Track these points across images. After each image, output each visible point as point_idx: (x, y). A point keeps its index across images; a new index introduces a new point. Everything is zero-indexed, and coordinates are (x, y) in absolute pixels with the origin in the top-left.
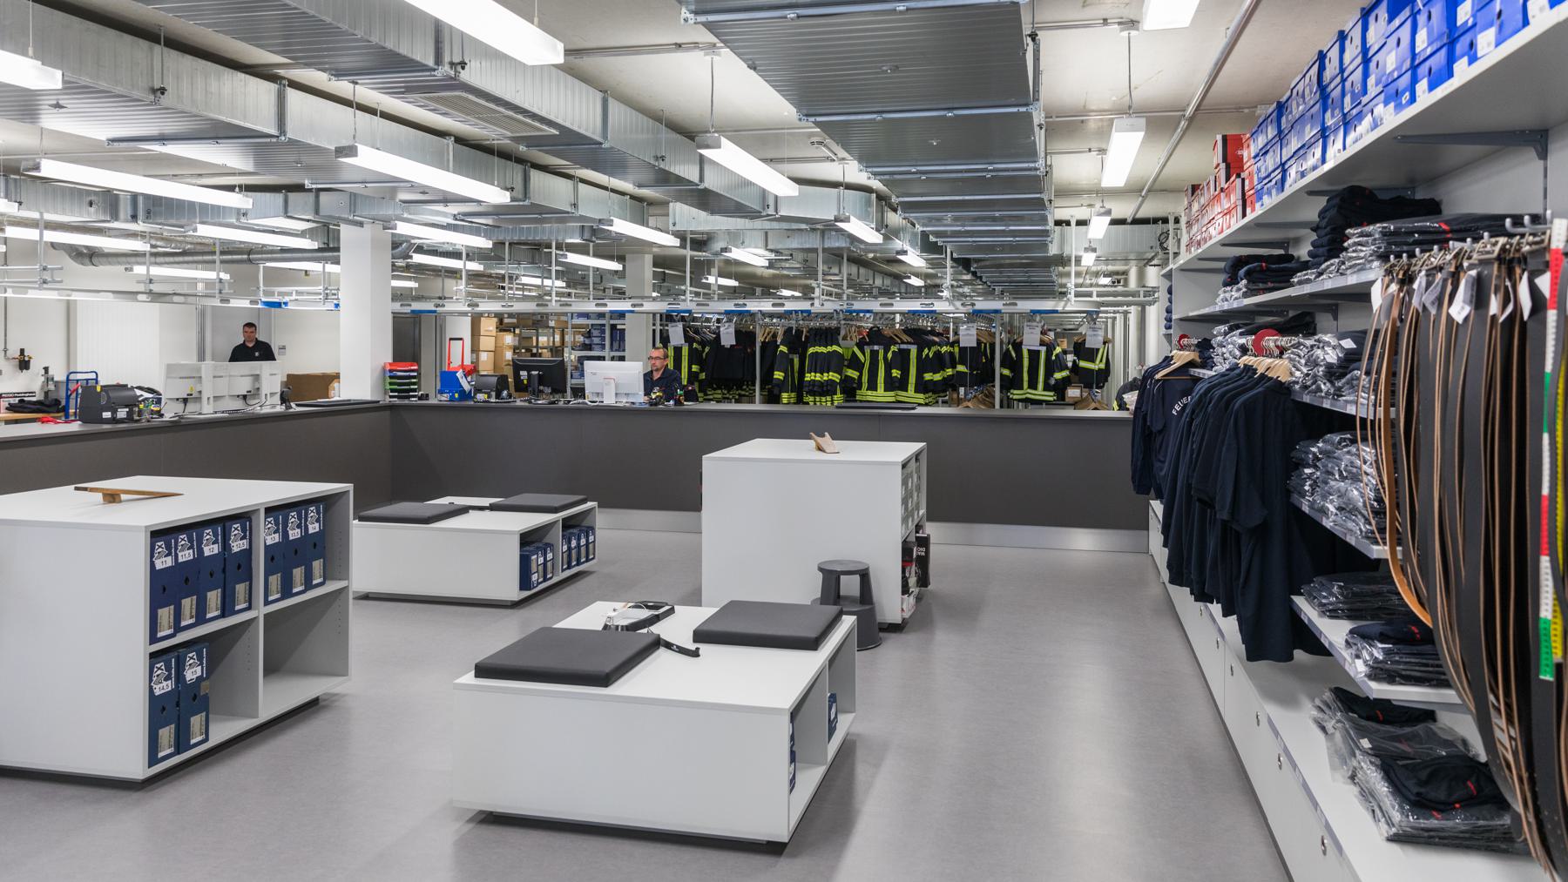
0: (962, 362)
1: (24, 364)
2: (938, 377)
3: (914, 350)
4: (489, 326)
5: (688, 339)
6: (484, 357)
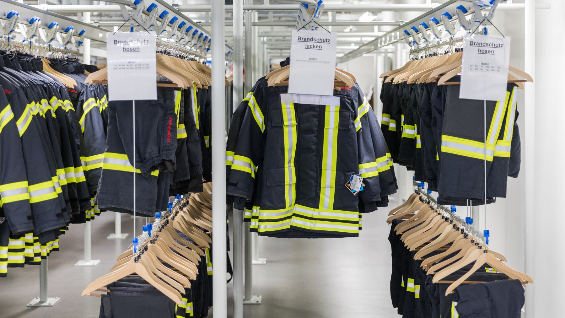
0: (117, 146)
2: (45, 192)
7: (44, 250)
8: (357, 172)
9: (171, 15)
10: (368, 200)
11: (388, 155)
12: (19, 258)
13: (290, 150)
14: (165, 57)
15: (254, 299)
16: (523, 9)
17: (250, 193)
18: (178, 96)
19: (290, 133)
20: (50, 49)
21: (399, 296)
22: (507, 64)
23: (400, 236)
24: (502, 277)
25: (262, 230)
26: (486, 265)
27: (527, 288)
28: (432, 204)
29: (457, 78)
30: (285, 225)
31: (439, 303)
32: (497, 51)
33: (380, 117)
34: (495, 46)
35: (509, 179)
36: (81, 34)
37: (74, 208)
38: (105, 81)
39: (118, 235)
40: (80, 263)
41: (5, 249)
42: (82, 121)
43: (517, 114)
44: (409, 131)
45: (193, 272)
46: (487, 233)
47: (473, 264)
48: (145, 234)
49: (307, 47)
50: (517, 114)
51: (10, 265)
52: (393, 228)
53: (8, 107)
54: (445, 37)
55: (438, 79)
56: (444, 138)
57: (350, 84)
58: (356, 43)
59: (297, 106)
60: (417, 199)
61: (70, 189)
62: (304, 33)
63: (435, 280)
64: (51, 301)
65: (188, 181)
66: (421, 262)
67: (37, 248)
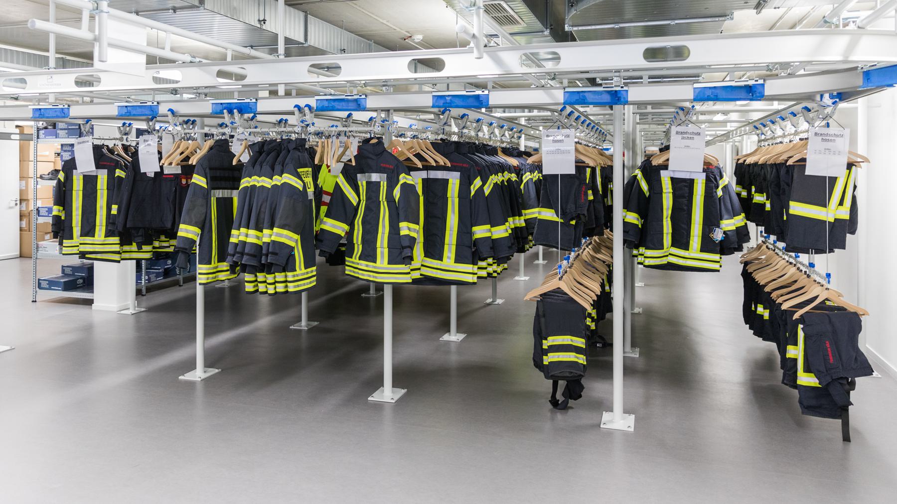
2: (501, 232)
3: (454, 180)
7: (499, 269)
8: (718, 226)
9: (583, 118)
10: (728, 246)
11: (743, 215)
12: (483, 273)
13: (668, 209)
14: (578, 145)
15: (637, 310)
16: (856, 108)
17: (641, 237)
18: (588, 170)
19: (668, 198)
20: (502, 142)
21: (750, 317)
22: (847, 149)
23: (751, 273)
24: (841, 309)
25: (646, 264)
26: (827, 299)
27: (863, 318)
28: (777, 251)
29: (804, 160)
30: (664, 261)
31: (786, 324)
32: (838, 139)
33: (735, 188)
34: (837, 136)
35: (848, 235)
36: (520, 131)
37: (519, 243)
38: (541, 161)
39: (541, 261)
40: (517, 278)
41: (476, 267)
42: (522, 187)
43: (855, 187)
44: (759, 198)
45: (598, 290)
46: (828, 275)
47: (816, 297)
48: (565, 262)
49: (683, 138)
50: (855, 187)
51: (478, 277)
52: (744, 267)
53: (479, 178)
54: (790, 129)
55: (787, 161)
56: (792, 204)
57: (715, 164)
58: (710, 135)
59: (672, 179)
60: (764, 247)
61: (516, 230)
62: (680, 129)
63: (784, 307)
64: (499, 301)
65: (594, 229)
66: (771, 293)
67: (495, 267)
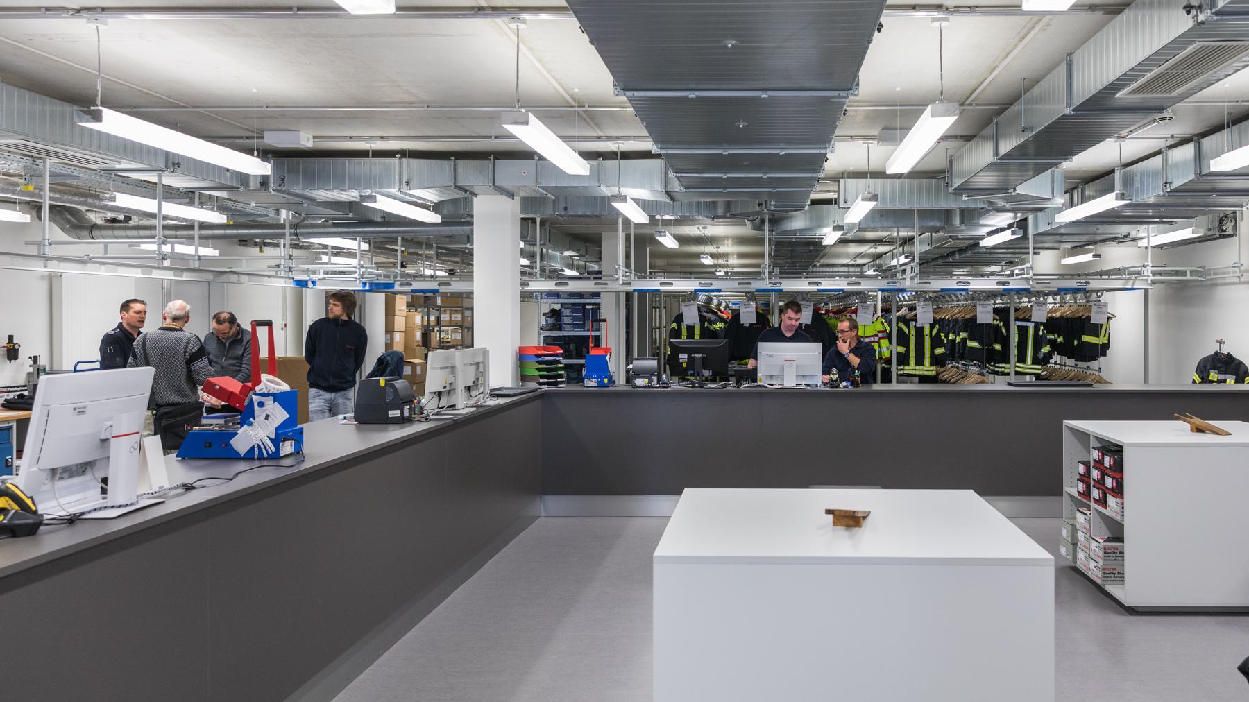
1: (12, 353)
4: (401, 303)
5: (702, 319)
6: (398, 337)
